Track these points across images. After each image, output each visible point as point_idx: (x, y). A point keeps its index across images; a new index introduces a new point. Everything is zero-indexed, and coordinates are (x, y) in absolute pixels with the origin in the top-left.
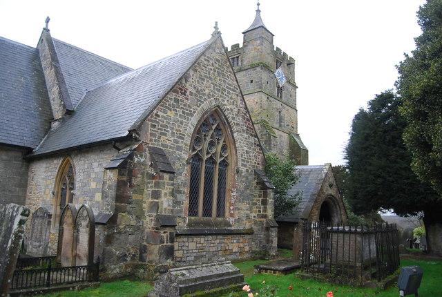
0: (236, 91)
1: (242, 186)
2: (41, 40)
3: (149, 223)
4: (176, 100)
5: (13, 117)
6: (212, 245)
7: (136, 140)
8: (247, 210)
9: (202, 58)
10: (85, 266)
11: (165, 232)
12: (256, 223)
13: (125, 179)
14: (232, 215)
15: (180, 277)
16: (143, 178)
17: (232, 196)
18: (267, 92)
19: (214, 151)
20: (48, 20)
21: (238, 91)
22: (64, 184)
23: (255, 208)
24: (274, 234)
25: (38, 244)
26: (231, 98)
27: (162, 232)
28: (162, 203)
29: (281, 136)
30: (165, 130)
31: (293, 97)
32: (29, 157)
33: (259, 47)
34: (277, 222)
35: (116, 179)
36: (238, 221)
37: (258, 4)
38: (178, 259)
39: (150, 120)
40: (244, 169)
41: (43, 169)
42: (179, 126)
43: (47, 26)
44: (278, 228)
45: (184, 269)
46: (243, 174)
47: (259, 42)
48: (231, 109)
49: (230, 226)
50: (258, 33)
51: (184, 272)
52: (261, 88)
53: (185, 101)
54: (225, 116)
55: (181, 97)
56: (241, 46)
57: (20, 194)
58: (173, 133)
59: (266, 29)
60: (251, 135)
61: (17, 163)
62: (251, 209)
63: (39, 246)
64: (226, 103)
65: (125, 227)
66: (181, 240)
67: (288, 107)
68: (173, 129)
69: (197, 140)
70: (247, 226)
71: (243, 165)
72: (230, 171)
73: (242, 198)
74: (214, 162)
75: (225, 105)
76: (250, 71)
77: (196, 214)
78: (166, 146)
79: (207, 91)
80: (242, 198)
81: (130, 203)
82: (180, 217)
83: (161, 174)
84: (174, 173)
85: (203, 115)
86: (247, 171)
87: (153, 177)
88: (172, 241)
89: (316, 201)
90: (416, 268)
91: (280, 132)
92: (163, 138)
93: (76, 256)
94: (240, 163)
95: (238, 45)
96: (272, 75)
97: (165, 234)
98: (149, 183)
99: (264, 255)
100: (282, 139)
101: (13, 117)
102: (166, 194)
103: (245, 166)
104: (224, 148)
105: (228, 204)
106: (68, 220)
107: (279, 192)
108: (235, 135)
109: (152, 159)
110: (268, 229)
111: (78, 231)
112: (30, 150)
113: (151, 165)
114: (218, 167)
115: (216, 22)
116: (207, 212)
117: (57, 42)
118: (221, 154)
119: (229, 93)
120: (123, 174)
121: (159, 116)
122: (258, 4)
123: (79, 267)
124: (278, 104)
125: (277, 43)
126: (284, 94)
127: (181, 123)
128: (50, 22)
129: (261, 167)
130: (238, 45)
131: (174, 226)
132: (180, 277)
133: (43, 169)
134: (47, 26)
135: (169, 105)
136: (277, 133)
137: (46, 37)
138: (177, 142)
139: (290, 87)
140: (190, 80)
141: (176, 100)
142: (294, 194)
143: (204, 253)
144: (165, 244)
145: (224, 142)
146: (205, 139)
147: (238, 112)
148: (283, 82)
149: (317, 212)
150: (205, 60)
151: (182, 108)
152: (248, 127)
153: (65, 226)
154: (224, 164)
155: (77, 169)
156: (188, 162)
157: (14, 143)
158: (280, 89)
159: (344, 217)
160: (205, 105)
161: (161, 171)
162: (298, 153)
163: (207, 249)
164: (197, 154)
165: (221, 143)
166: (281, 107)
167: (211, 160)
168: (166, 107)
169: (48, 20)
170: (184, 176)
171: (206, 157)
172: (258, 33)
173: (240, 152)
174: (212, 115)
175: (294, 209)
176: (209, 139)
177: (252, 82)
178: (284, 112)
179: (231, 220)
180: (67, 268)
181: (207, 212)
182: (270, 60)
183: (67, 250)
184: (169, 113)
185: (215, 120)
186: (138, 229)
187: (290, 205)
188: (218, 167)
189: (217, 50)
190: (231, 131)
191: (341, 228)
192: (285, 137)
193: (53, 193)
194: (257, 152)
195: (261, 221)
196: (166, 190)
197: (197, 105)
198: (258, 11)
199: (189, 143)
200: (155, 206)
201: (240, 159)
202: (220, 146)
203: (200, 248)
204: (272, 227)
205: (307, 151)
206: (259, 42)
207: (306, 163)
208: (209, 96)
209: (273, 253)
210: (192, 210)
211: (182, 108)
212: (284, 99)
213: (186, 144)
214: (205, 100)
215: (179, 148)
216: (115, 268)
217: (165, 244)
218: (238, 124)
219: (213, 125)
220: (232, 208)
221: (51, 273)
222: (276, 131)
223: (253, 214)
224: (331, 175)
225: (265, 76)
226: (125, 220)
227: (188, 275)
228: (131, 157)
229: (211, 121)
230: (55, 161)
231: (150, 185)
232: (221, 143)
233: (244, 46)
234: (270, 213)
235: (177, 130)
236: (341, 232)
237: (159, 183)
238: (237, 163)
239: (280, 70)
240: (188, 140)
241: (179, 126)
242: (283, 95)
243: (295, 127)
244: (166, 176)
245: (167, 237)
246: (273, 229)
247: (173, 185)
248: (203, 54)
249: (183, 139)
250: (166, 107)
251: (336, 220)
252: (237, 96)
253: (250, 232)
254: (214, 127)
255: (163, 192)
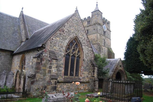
0: (84, 31)
1: (85, 65)
2: (20, 15)
3: (48, 78)
4: (60, 34)
5: (8, 40)
6: (73, 86)
7: (45, 48)
8: (87, 74)
9: (71, 19)
10: (22, 92)
11: (53, 81)
12: (90, 79)
13: (39, 61)
14: (81, 76)
15: (51, 98)
16: (46, 61)
17: (82, 68)
18: (100, 33)
19: (75, 53)
20: (22, 9)
21: (85, 31)
22: (23, 63)
23: (90, 74)
24: (97, 83)
25: (9, 84)
26: (82, 34)
27: (52, 81)
28: (52, 70)
29: (105, 49)
30: (55, 45)
31: (109, 35)
32: (12, 54)
33: (97, 17)
34: (98, 79)
35: (36, 61)
36: (84, 78)
37: (97, 3)
38: (59, 91)
39: (50, 41)
40: (86, 59)
41: (17, 58)
42: (61, 43)
43: (22, 10)
44: (99, 81)
45: (54, 95)
46: (86, 61)
47: (97, 15)
48: (82, 38)
49: (80, 80)
50: (97, 13)
51: (54, 96)
52: (97, 32)
53: (64, 34)
54: (79, 40)
55: (62, 33)
56: (91, 17)
57: (10, 67)
58: (58, 46)
59: (100, 11)
60: (89, 47)
61: (9, 56)
62: (89, 74)
63: (10, 85)
64: (80, 35)
65: (39, 79)
66: (61, 84)
67: (108, 39)
68: (58, 44)
69: (68, 48)
70: (87, 80)
71: (86, 58)
72: (81, 60)
73: (85, 70)
74: (75, 57)
75: (79, 36)
76: (94, 26)
77: (67, 75)
78: (56, 50)
79: (72, 31)
80: (85, 70)
81: (41, 70)
82: (60, 76)
83: (52, 60)
84: (57, 60)
85: (71, 40)
86: (87, 60)
87: (50, 61)
88: (56, 84)
89: (114, 72)
90: (138, 99)
91: (105, 47)
92: (55, 47)
93: (20, 89)
94: (84, 57)
95: (90, 17)
96: (101, 27)
97: (53, 82)
98: (48, 63)
99: (93, 91)
100: (105, 50)
101: (8, 40)
102: (54, 67)
103: (87, 58)
104: (79, 51)
105: (80, 72)
106: (18, 76)
107: (100, 68)
108: (83, 47)
109: (50, 55)
110: (95, 81)
111: (21, 79)
112: (13, 52)
113: (49, 57)
114: (76, 58)
115: (77, 7)
116: (71, 75)
117: (25, 16)
118: (72, 52)
119: (81, 32)
120: (39, 60)
121: (53, 39)
122: (97, 3)
123: (20, 92)
124: (104, 37)
125: (104, 16)
126: (106, 34)
127: (62, 42)
128: (23, 9)
129: (93, 59)
130: (90, 17)
131: (57, 79)
132: (85, 85)
133: (17, 58)
134: (22, 10)
135: (57, 36)
136: (103, 48)
137: (22, 15)
138: (60, 49)
139: (108, 31)
140: (66, 27)
141: (60, 34)
142: (106, 69)
143: (70, 89)
144: (53, 85)
145: (79, 49)
146: (76, 50)
147: (84, 39)
148: (106, 30)
149: (115, 76)
150: (72, 20)
151: (62, 37)
152: (88, 44)
153: (17, 78)
154: (79, 57)
155: (26, 58)
156: (64, 56)
157: (8, 49)
158: (105, 32)
159: (126, 78)
160: (72, 36)
161: (52, 59)
162: (111, 54)
163: (71, 88)
164: (68, 54)
165: (78, 50)
166: (105, 38)
167: (74, 56)
168: (56, 36)
169: (22, 9)
170: (62, 61)
171: (71, 55)
172: (97, 13)
173: (85, 53)
174: (74, 40)
175: (106, 75)
176: (73, 48)
177: (94, 29)
178: (106, 40)
179: (81, 78)
180: (17, 92)
181: (71, 75)
182: (101, 22)
183: (17, 87)
184: (57, 38)
185: (75, 41)
186: (44, 80)
187: (104, 73)
188: (76, 58)
189: (76, 17)
190: (81, 45)
191: (129, 82)
192: (106, 49)
193: (19, 66)
194: (92, 53)
195: (92, 78)
196: (54, 66)
197: (68, 36)
198: (97, 5)
199: (65, 49)
200: (50, 72)
201: (85, 56)
202: (77, 51)
203: (68, 87)
204: (96, 80)
205: (114, 54)
206: (97, 15)
207: (114, 58)
208: (73, 33)
209: (96, 90)
210: (66, 73)
211: (62, 37)
212: (106, 36)
213: (63, 50)
214: (72, 34)
215: (60, 51)
216: (34, 93)
217: (53, 85)
218: (84, 43)
219: (74, 43)
220: (81, 73)
221: (8, 95)
222: (103, 47)
223: (89, 76)
224: (120, 62)
225: (99, 27)
226: (38, 76)
227: (54, 97)
228: (42, 53)
229: (74, 41)
230: (20, 56)
231: (48, 64)
232: (78, 50)
233: (92, 17)
234: (96, 75)
235: (60, 45)
236: (121, 83)
237: (51, 63)
238: (83, 57)
239: (104, 25)
240: (64, 48)
241: (61, 43)
242: (106, 34)
243: (110, 46)
244: (54, 61)
245: (54, 83)
246: (96, 81)
247: (57, 64)
248: (71, 18)
249: (62, 48)
250: (56, 36)
251: (123, 79)
252: (84, 33)
253: (88, 82)
254: (75, 44)
255: (53, 66)
